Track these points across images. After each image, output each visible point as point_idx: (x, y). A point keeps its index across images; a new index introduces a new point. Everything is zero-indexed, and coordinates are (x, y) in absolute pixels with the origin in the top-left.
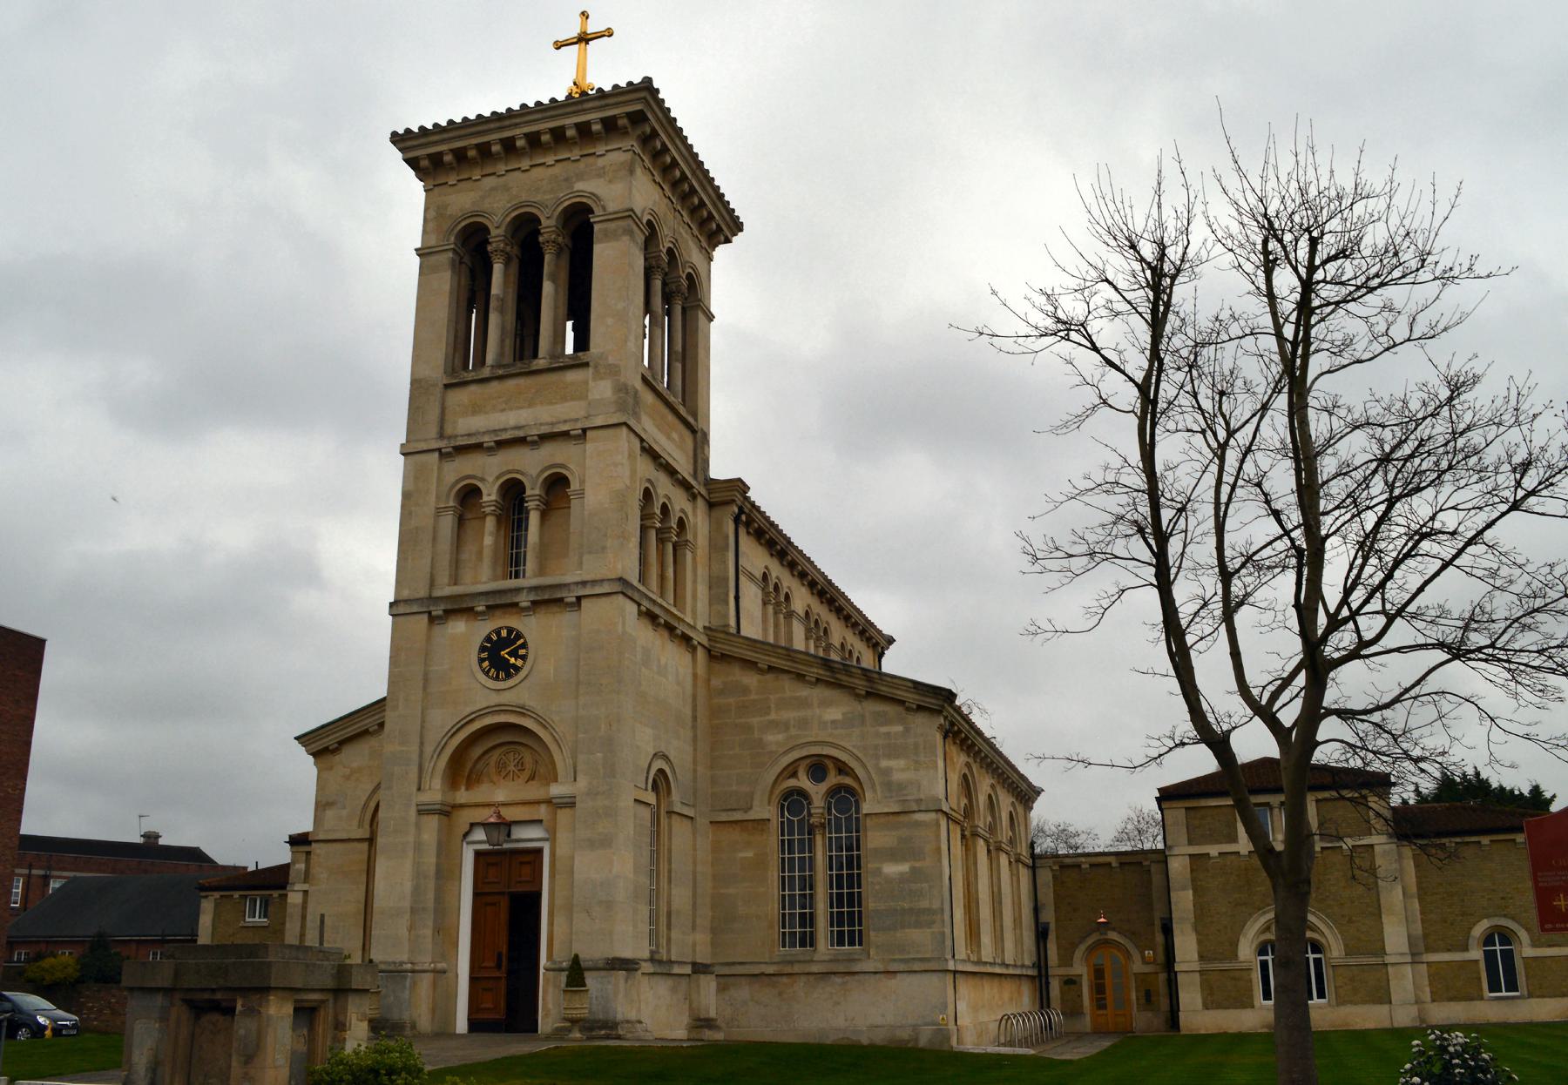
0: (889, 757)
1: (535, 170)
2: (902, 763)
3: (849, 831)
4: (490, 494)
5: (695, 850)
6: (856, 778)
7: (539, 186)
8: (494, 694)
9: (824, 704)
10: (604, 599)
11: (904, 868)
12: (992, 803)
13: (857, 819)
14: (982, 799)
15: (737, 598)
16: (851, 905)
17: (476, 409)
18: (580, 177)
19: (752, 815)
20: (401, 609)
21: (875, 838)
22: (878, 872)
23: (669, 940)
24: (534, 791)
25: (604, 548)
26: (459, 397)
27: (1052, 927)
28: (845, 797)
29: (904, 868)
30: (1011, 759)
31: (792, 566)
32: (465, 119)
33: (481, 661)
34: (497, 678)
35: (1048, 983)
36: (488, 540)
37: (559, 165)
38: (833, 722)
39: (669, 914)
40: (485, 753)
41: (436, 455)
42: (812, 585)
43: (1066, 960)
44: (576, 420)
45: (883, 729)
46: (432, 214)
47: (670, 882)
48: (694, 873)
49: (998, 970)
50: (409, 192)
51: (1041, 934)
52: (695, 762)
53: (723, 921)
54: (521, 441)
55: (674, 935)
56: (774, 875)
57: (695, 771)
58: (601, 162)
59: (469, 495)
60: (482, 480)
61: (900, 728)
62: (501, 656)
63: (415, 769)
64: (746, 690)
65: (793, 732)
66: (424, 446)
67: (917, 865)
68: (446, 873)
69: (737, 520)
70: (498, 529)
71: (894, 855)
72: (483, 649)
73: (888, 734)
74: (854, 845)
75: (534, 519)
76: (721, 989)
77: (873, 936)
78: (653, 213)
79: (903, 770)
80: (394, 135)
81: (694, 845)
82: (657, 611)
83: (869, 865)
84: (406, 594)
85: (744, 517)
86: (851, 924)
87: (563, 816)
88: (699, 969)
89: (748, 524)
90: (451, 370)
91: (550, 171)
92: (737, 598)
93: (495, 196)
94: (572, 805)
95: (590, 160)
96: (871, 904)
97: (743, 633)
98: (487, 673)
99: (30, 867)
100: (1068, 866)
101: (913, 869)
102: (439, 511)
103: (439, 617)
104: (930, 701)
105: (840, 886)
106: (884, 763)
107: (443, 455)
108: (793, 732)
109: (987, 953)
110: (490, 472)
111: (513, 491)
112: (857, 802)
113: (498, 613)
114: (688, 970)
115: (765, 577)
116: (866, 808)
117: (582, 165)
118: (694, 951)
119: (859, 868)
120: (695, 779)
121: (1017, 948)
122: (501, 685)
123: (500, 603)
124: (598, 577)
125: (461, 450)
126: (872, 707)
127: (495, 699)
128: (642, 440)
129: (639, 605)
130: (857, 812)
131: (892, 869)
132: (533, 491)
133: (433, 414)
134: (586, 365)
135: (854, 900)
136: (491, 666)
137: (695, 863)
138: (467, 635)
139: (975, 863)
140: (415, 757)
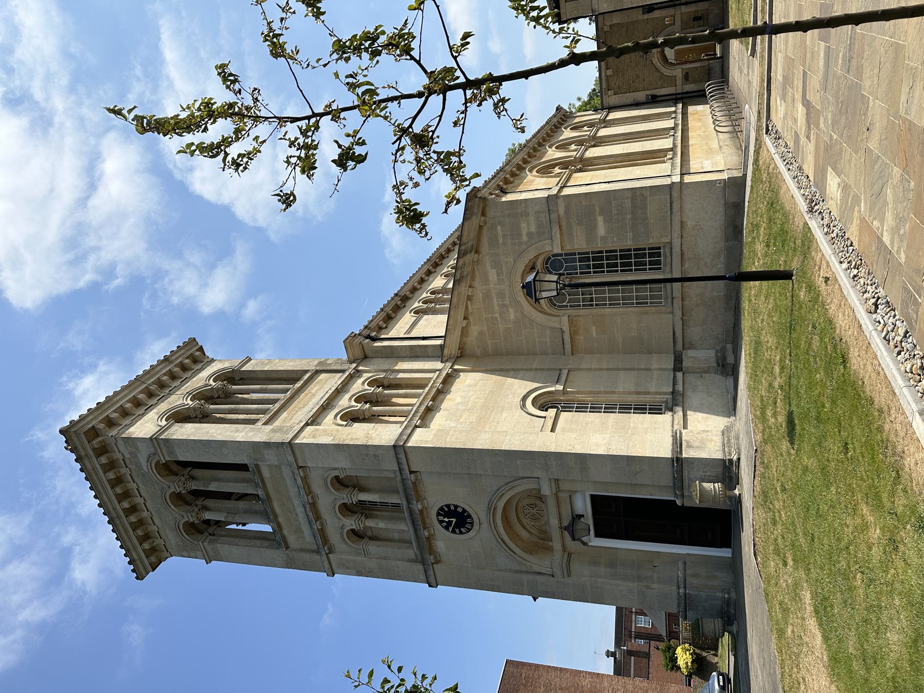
0: (520, 235)
1: (143, 495)
2: (524, 225)
3: (574, 261)
4: (350, 523)
5: (590, 369)
6: (537, 257)
7: (153, 495)
8: (482, 526)
9: (486, 281)
10: (409, 456)
11: (600, 220)
12: (563, 146)
13: (566, 255)
14: (559, 154)
15: (424, 338)
16: (629, 257)
17: (298, 531)
18: (139, 467)
19: (566, 328)
20: (433, 582)
21: (580, 244)
22: (603, 239)
23: (657, 393)
24: (551, 503)
25: (375, 456)
26: (292, 539)
27: (648, 92)
28: (553, 263)
29: (600, 220)
30: (417, 327)
31: (414, 290)
32: (117, 539)
33: (461, 533)
34: (472, 524)
35: (687, 93)
36: (382, 525)
37: (136, 480)
38: (498, 275)
39: (638, 393)
40: (524, 527)
41: (331, 556)
42: (429, 273)
43: (672, 81)
44: (293, 473)
45: (501, 240)
46: (185, 553)
47: (614, 393)
48: (608, 369)
49: (679, 134)
50: (174, 565)
51: (654, 101)
52: (531, 370)
53: (640, 347)
54: (314, 505)
55: (653, 390)
56: (608, 311)
57: (536, 370)
58: (127, 456)
59: (357, 535)
60: (342, 528)
61: (499, 227)
62: (457, 519)
63: (539, 578)
64: (481, 333)
65: (507, 302)
66: (326, 563)
67: (598, 210)
68: (613, 560)
69: (374, 339)
70: (376, 517)
71: (591, 229)
72: (441, 509)
73: (504, 236)
74: (584, 258)
75: (364, 497)
76: (692, 346)
77: (653, 241)
78: (161, 417)
79: (528, 225)
80: (137, 578)
81: (587, 369)
82: (423, 408)
83: (599, 246)
84: (423, 577)
85: (373, 334)
86: (644, 256)
87: (564, 486)
88: (678, 366)
89: (380, 329)
90: (279, 546)
91: (141, 486)
92: (424, 338)
93: (166, 520)
94: (557, 480)
95: (127, 461)
96: (629, 243)
97: (443, 334)
98: (469, 530)
99: (631, 612)
100: (608, 85)
101: (601, 214)
102: (366, 554)
103: (435, 557)
104: (477, 210)
105: (616, 265)
106: (525, 238)
107: (331, 551)
108: (507, 302)
109: (666, 143)
110: (337, 525)
111: (347, 509)
112: (554, 255)
113: (428, 521)
114: (679, 375)
115: (416, 312)
116: (557, 250)
117: (133, 467)
118: (665, 370)
119: (601, 252)
120: (542, 370)
121: (664, 119)
122: (476, 521)
123: (417, 521)
124: (395, 460)
125: (325, 540)
126: (485, 248)
127: (485, 526)
128: (307, 424)
129: (416, 427)
130: (561, 255)
131: (601, 230)
132: (346, 497)
133: (306, 556)
134: (257, 466)
135: (625, 254)
136: (464, 527)
137: (601, 369)
138: (444, 541)
139: (601, 157)
140: (531, 577)
